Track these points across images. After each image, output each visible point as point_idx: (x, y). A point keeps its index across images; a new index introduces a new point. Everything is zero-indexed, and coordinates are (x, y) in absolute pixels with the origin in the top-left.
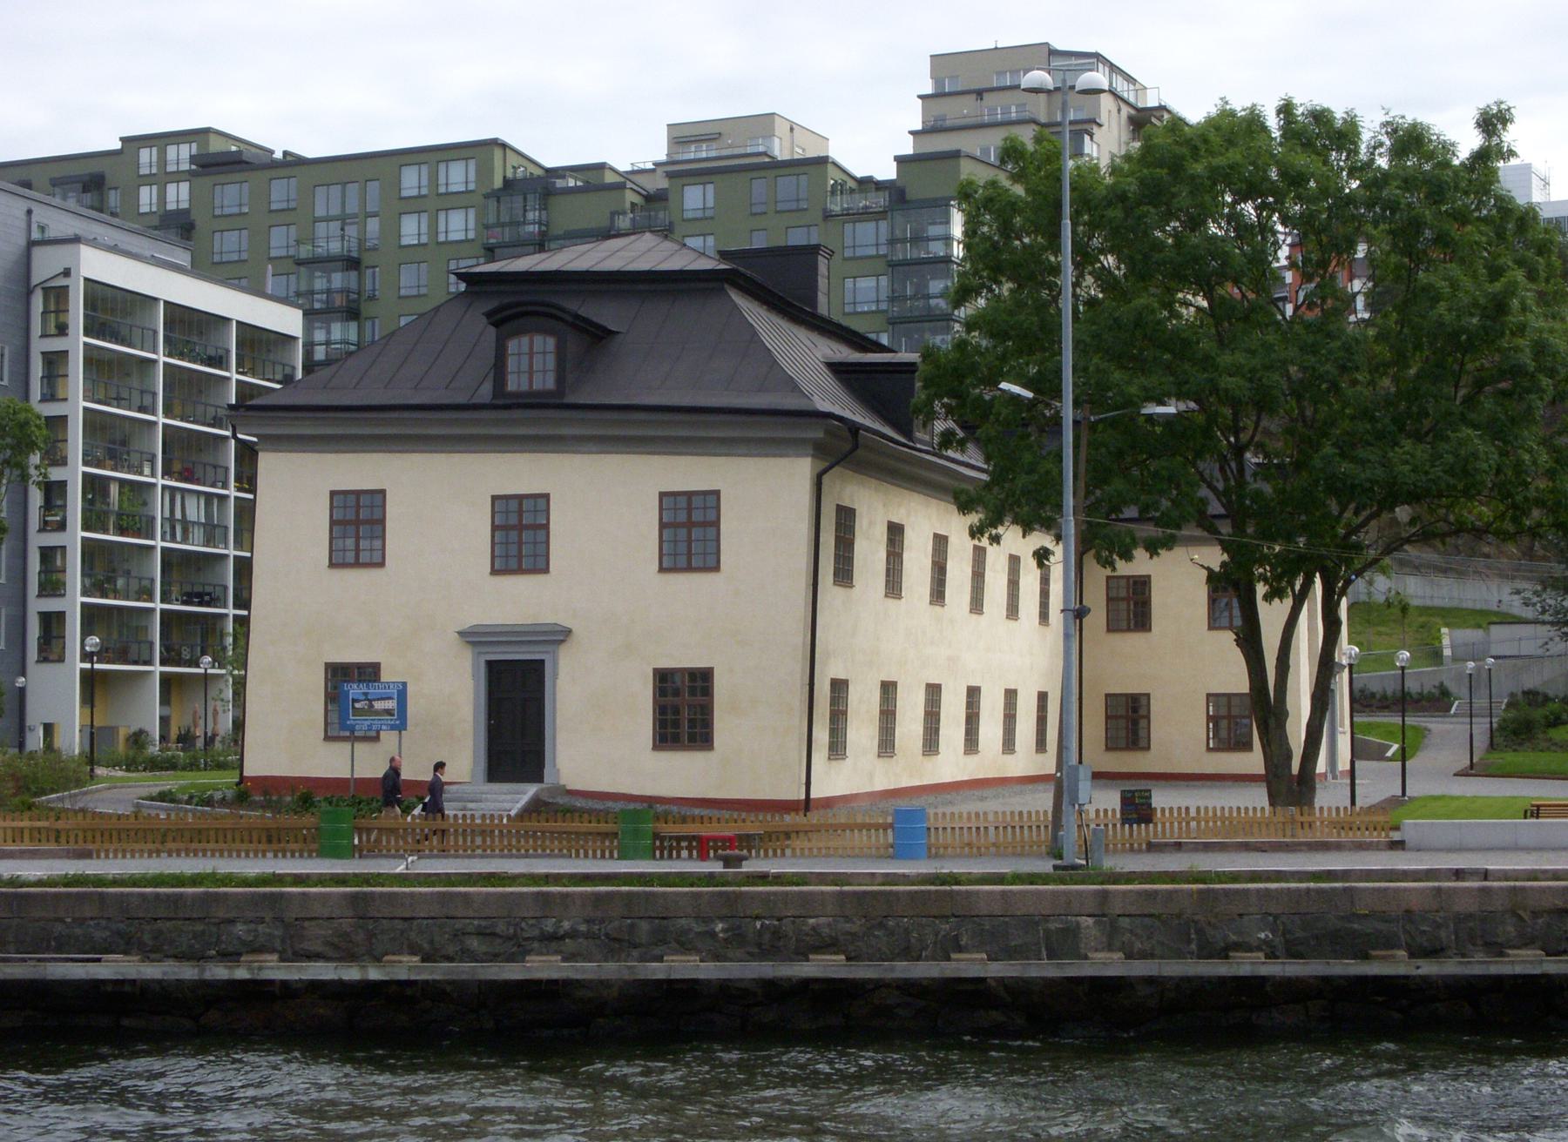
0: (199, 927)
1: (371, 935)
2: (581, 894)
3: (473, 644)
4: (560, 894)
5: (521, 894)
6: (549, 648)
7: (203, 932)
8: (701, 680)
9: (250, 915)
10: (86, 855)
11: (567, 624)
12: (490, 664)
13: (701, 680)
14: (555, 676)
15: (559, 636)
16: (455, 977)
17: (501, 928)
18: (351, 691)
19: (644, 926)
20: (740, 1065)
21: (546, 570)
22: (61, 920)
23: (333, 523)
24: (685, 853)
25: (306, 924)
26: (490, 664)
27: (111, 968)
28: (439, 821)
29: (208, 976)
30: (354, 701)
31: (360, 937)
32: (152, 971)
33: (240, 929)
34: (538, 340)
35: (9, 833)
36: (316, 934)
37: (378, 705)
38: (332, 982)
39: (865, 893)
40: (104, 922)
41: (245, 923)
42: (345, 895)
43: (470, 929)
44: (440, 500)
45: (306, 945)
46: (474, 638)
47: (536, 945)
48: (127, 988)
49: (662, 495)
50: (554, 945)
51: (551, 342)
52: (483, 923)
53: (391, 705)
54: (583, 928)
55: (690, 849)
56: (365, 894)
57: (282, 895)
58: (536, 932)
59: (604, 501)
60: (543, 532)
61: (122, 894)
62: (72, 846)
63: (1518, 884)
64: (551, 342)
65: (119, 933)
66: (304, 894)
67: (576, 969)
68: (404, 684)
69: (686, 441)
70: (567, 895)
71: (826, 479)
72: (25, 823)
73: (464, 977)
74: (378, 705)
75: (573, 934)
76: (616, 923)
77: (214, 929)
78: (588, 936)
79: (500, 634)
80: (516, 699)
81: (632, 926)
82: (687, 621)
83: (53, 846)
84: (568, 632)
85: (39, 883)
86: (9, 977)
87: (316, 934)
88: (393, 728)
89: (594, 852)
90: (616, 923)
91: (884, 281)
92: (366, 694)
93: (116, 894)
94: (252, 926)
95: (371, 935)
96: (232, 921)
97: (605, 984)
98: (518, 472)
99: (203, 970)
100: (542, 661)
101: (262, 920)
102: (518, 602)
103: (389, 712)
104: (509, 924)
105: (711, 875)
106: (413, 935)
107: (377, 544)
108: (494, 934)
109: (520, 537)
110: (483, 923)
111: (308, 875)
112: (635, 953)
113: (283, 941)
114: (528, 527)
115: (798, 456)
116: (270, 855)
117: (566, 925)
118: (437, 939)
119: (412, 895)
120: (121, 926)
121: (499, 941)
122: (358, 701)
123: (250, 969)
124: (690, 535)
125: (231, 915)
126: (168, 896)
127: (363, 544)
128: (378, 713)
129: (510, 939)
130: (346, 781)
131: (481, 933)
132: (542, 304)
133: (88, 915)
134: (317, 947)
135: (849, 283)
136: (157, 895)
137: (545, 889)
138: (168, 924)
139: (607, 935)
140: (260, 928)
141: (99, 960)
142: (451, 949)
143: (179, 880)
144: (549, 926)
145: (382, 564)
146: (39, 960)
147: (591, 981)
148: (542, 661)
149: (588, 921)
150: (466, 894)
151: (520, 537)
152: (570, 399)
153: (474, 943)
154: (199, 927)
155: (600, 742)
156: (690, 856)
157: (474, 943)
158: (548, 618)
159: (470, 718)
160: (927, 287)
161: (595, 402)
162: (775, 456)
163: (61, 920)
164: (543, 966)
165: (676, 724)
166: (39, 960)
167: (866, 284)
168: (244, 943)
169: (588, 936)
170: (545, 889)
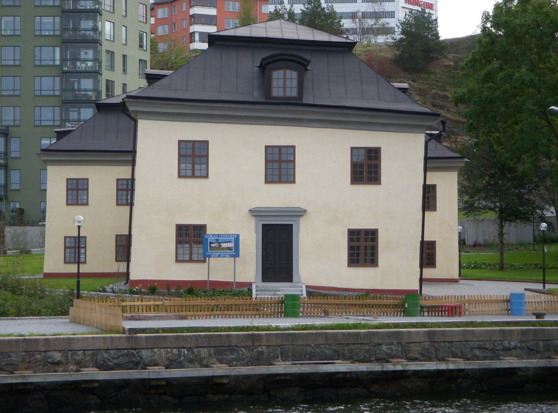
0: (367, 347)
1: (437, 350)
2: (517, 330)
3: (256, 216)
4: (509, 330)
5: (494, 330)
6: (295, 219)
7: (369, 349)
8: (371, 235)
9: (388, 341)
10: (184, 318)
11: (303, 206)
12: (264, 226)
13: (371, 235)
14: (298, 231)
15: (300, 213)
16: (483, 367)
17: (488, 345)
18: (191, 238)
19: (541, 344)
20: (480, 408)
21: (294, 182)
22: (310, 346)
23: (180, 156)
24: (426, 314)
25: (411, 345)
26: (264, 226)
27: (341, 367)
28: (249, 300)
29: (385, 369)
30: (210, 243)
31: (432, 350)
32: (363, 367)
33: (384, 348)
34: (288, 72)
35: (144, 308)
36: (415, 350)
37: (224, 245)
38: (435, 370)
39: (309, 333)
40: (327, 346)
41: (386, 345)
42: (425, 332)
43: (475, 346)
44: (238, 149)
45: (411, 355)
46: (256, 213)
47: (501, 352)
48: (348, 376)
49: (352, 149)
50: (508, 352)
51: (295, 74)
52: (481, 343)
53: (231, 245)
54: (519, 345)
55: (428, 312)
56: (433, 331)
57: (400, 332)
58: (501, 347)
59: (324, 152)
60: (292, 164)
61: (334, 333)
62: (176, 313)
63: (85, 336)
64: (295, 74)
65: (336, 351)
66: (409, 331)
67: (529, 362)
68: (238, 235)
69: (364, 123)
70: (512, 330)
71: (429, 143)
72: (151, 303)
73: (486, 367)
74: (224, 245)
75: (515, 348)
76: (531, 343)
77: (373, 348)
78: (522, 348)
79: (285, 211)
80: (278, 244)
81: (537, 344)
82: (364, 206)
83: (164, 314)
84: (305, 211)
85: (293, 329)
86: (303, 372)
87: (415, 350)
88: (231, 256)
89: (390, 313)
90: (531, 343)
91: (58, 19)
92: (217, 240)
93: (332, 333)
94: (389, 346)
95: (437, 350)
96: (380, 344)
97: (527, 368)
98: (194, 131)
99: (383, 367)
100: (291, 225)
101: (393, 344)
102: (279, 197)
103: (229, 249)
104: (490, 344)
105: (529, 322)
106: (454, 349)
107: (204, 167)
108: (486, 348)
109: (280, 165)
110: (481, 343)
111: (398, 323)
112: (538, 356)
113: (402, 353)
114: (284, 161)
115: (419, 133)
116: (257, 316)
117: (513, 344)
118: (464, 350)
119: (451, 331)
120: (336, 347)
121: (487, 351)
122: (213, 243)
123: (402, 365)
124: (366, 168)
125: (380, 342)
126: (354, 333)
127: (197, 167)
128: (223, 249)
129: (491, 350)
130: (205, 282)
131: (480, 348)
132: (296, 56)
133: (321, 343)
134: (416, 355)
135: (38, 19)
136: (349, 333)
137: (503, 328)
138: (355, 346)
139: (528, 348)
140: (393, 347)
141: (333, 363)
142: (469, 355)
143: (216, 329)
144: (506, 344)
145: (207, 176)
146: (316, 364)
147: (523, 368)
148: (291, 225)
149: (520, 342)
150: (473, 331)
151: (280, 165)
152: (305, 101)
153: (477, 352)
154: (367, 347)
155: (320, 262)
156: (428, 315)
157: (477, 352)
158: (294, 204)
159: (254, 251)
160: (79, 24)
161: (341, 105)
162: (270, 125)
163: (310, 346)
164: (509, 362)
165: (358, 255)
166: (316, 364)
167: (48, 20)
168: (387, 354)
169: (522, 348)
170: (503, 328)
